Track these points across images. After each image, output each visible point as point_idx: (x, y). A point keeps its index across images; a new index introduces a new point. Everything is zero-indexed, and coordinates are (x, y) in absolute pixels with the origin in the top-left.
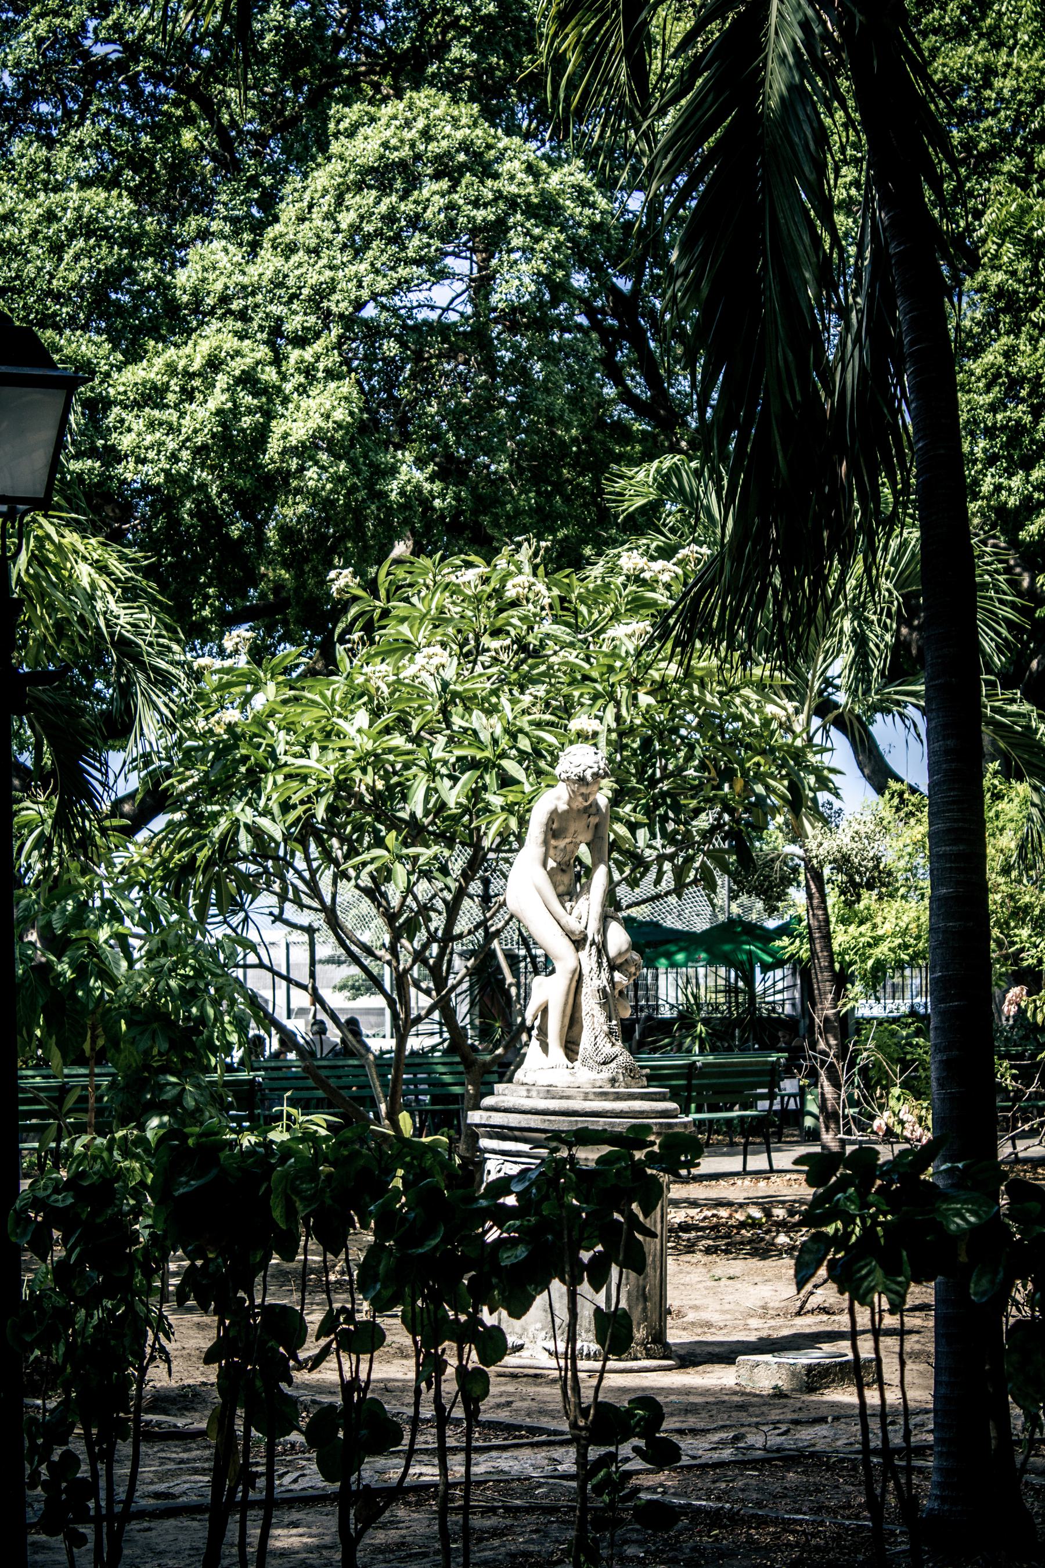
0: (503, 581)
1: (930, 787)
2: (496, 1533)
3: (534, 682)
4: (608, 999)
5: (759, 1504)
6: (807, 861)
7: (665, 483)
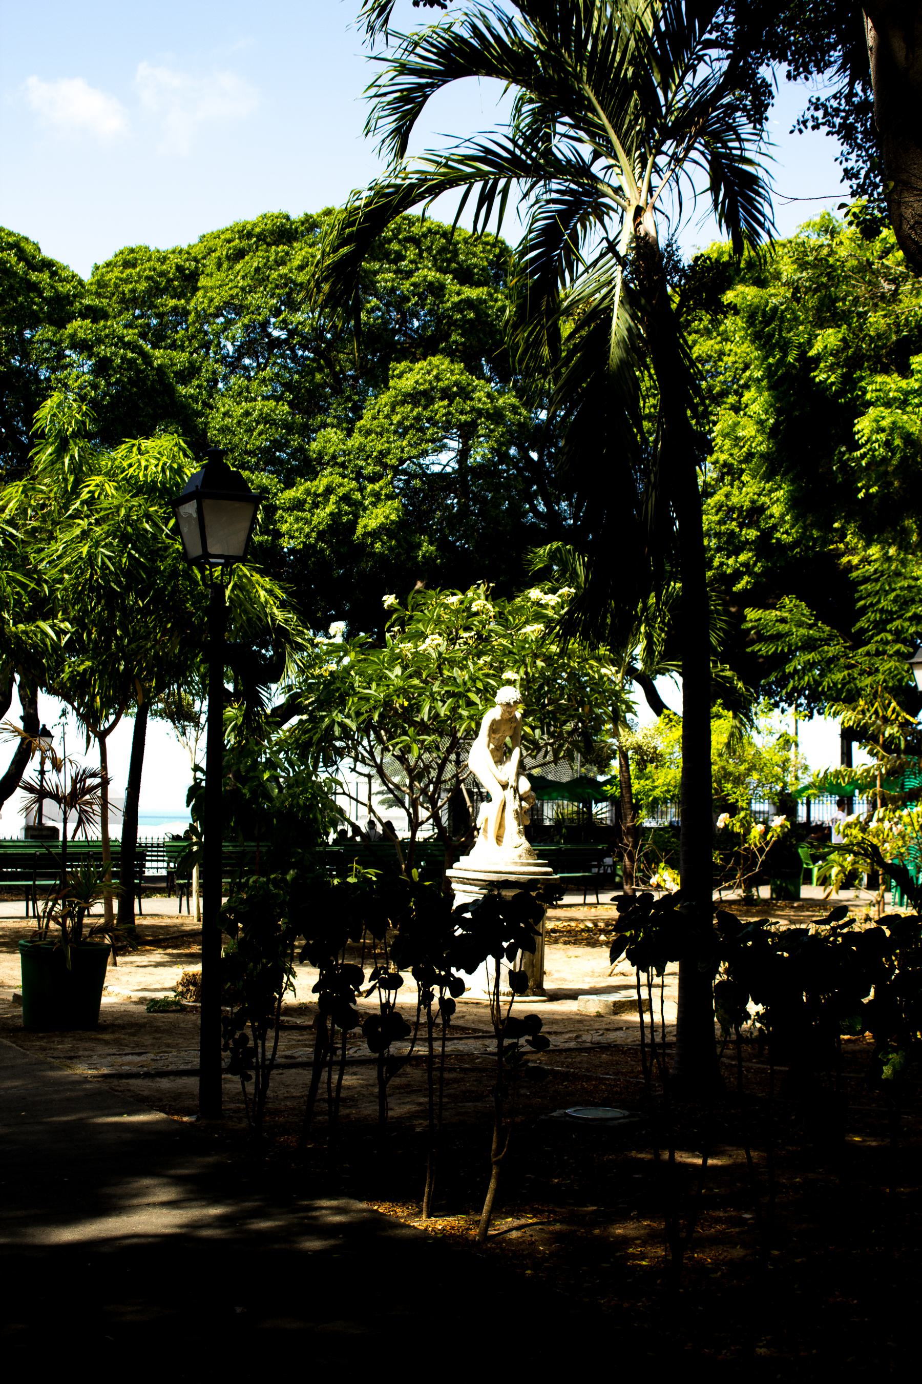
0: (471, 603)
1: (684, 713)
2: (455, 1081)
3: (485, 654)
4: (519, 815)
5: (587, 1070)
6: (620, 748)
7: (553, 556)
